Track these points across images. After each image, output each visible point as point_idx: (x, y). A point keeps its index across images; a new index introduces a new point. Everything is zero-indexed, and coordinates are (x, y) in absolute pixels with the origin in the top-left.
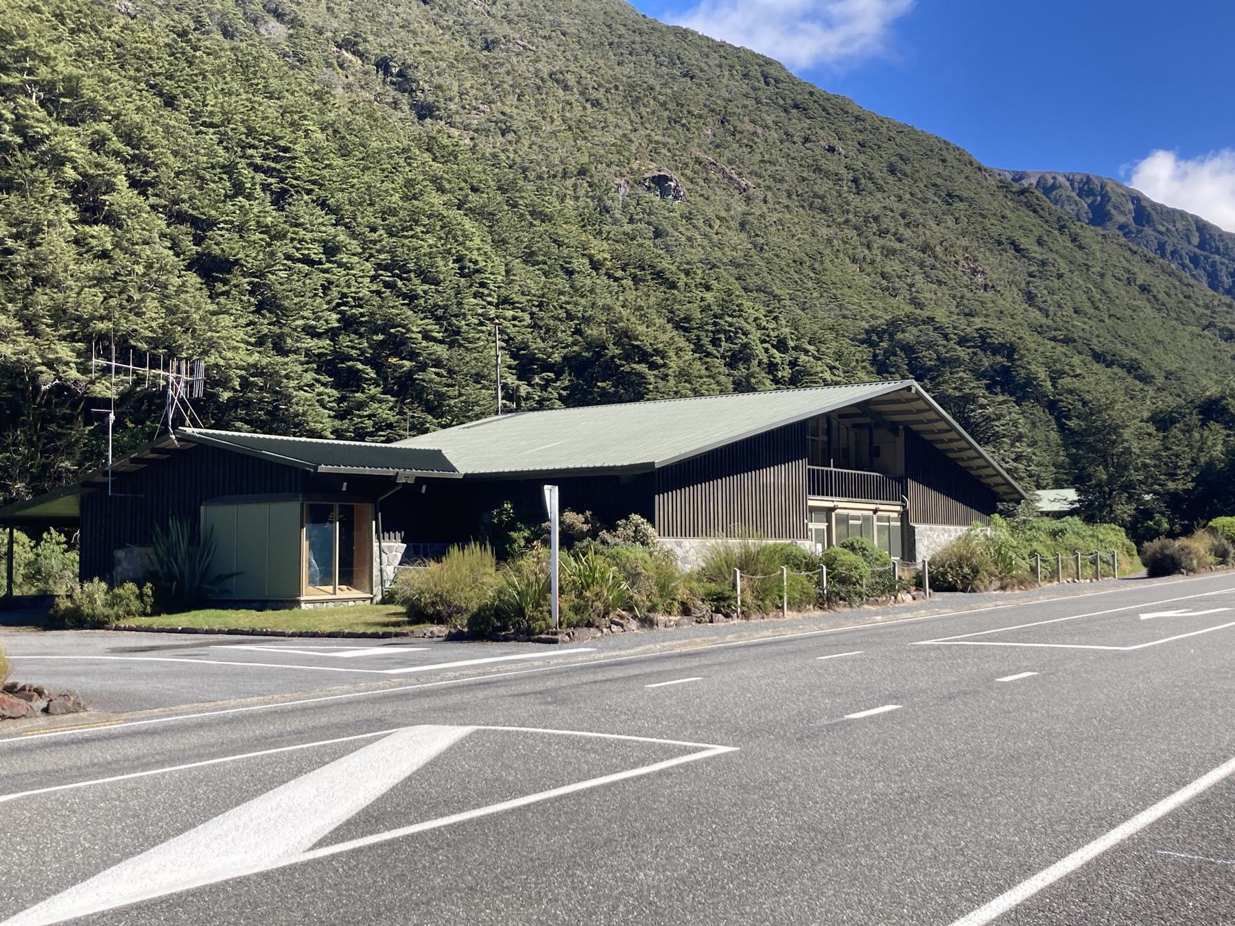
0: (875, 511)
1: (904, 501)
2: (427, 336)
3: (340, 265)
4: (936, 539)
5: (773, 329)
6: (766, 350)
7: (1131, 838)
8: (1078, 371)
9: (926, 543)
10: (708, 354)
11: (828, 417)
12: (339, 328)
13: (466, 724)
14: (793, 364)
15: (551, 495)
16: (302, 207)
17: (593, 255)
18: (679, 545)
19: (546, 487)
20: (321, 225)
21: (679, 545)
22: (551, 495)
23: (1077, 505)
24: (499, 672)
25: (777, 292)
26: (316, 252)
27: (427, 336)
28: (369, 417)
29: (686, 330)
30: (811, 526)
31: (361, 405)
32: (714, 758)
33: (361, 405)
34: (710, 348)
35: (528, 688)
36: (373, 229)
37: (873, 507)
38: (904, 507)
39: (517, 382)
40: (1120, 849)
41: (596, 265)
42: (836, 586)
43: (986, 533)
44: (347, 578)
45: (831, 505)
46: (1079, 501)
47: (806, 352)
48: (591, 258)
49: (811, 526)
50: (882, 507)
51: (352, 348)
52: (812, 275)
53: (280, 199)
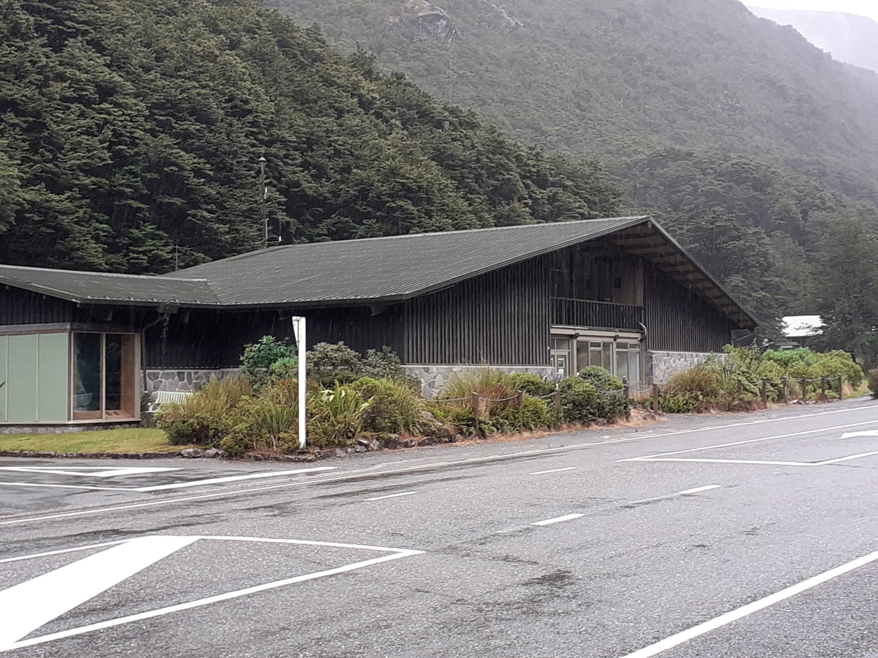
0: (615, 338)
1: (642, 329)
2: (198, 173)
3: (117, 105)
4: (674, 364)
5: (533, 166)
6: (527, 186)
7: (730, 624)
8: (829, 204)
9: (663, 367)
10: (472, 191)
11: (570, 250)
12: (114, 166)
13: (192, 535)
14: (552, 199)
15: (300, 325)
16: (74, 47)
17: (363, 96)
18: (427, 370)
19: (294, 318)
20: (98, 67)
21: (427, 370)
22: (300, 325)
23: (821, 332)
24: (254, 487)
25: (546, 128)
26: (90, 91)
27: (198, 173)
28: (144, 253)
29: (448, 167)
30: (553, 352)
31: (137, 242)
32: (400, 559)
33: (137, 242)
34: (475, 186)
35: (261, 502)
36: (147, 70)
37: (613, 334)
38: (643, 334)
39: (288, 219)
40: (718, 631)
41: (365, 104)
42: (589, 410)
43: (725, 361)
44: (114, 403)
45: (573, 332)
46: (821, 328)
47: (565, 187)
48: (360, 96)
49: (553, 352)
50: (621, 334)
51: (128, 186)
52: (578, 111)
53: (57, 44)
